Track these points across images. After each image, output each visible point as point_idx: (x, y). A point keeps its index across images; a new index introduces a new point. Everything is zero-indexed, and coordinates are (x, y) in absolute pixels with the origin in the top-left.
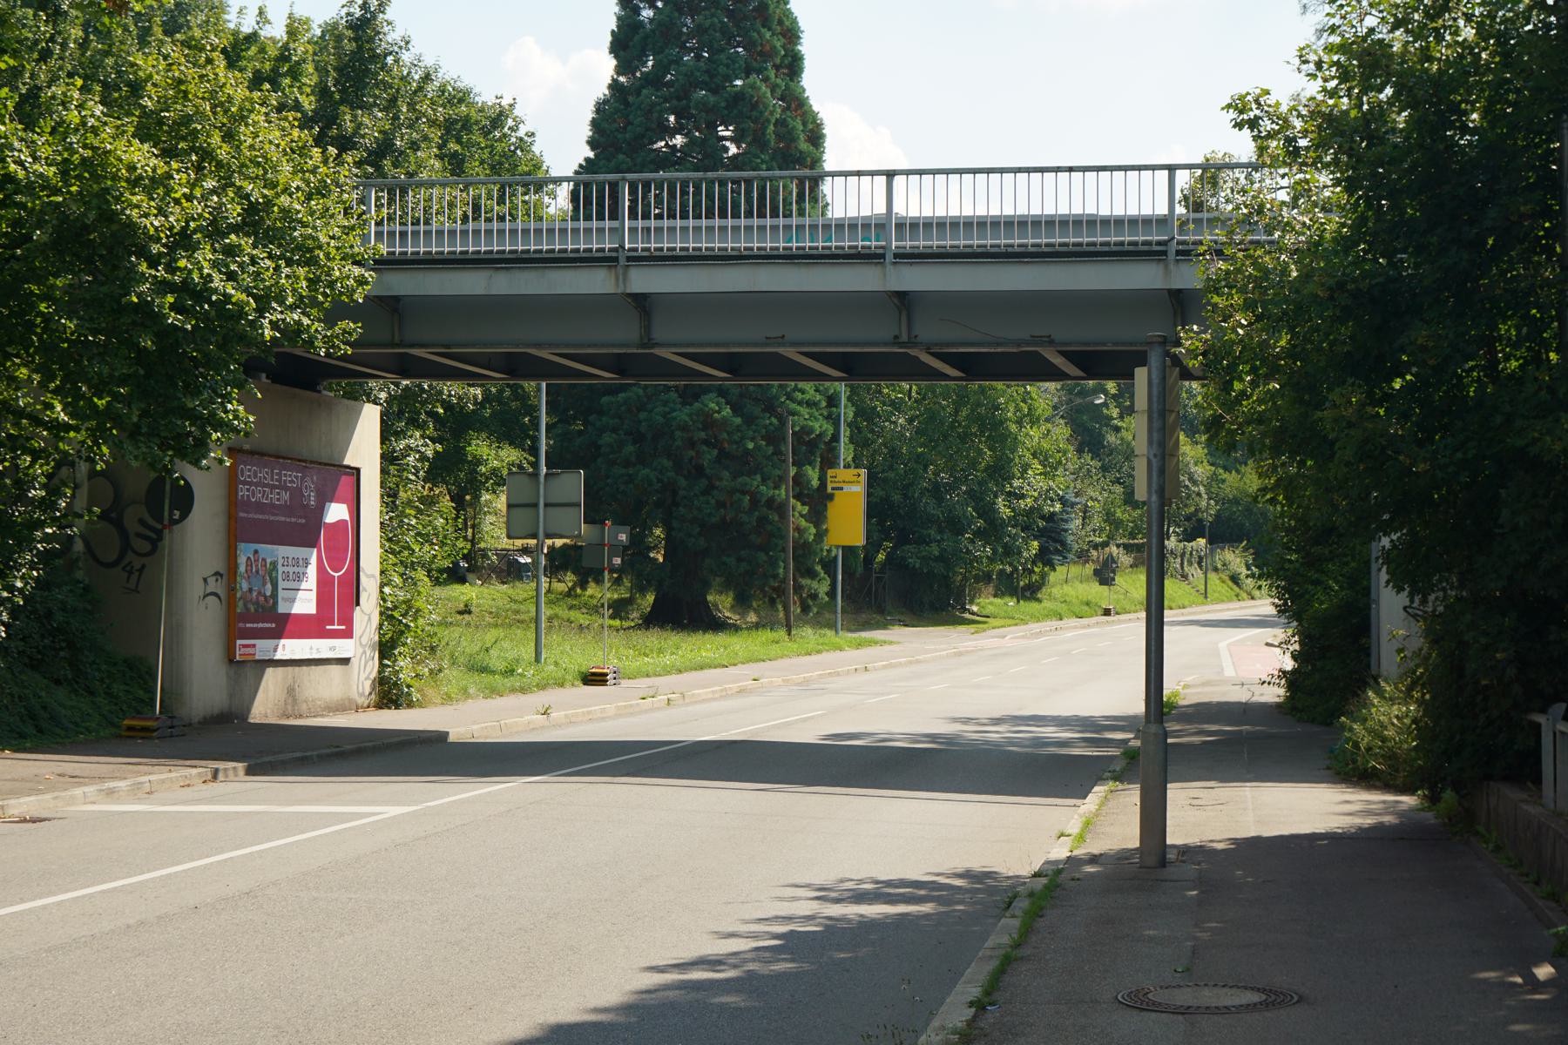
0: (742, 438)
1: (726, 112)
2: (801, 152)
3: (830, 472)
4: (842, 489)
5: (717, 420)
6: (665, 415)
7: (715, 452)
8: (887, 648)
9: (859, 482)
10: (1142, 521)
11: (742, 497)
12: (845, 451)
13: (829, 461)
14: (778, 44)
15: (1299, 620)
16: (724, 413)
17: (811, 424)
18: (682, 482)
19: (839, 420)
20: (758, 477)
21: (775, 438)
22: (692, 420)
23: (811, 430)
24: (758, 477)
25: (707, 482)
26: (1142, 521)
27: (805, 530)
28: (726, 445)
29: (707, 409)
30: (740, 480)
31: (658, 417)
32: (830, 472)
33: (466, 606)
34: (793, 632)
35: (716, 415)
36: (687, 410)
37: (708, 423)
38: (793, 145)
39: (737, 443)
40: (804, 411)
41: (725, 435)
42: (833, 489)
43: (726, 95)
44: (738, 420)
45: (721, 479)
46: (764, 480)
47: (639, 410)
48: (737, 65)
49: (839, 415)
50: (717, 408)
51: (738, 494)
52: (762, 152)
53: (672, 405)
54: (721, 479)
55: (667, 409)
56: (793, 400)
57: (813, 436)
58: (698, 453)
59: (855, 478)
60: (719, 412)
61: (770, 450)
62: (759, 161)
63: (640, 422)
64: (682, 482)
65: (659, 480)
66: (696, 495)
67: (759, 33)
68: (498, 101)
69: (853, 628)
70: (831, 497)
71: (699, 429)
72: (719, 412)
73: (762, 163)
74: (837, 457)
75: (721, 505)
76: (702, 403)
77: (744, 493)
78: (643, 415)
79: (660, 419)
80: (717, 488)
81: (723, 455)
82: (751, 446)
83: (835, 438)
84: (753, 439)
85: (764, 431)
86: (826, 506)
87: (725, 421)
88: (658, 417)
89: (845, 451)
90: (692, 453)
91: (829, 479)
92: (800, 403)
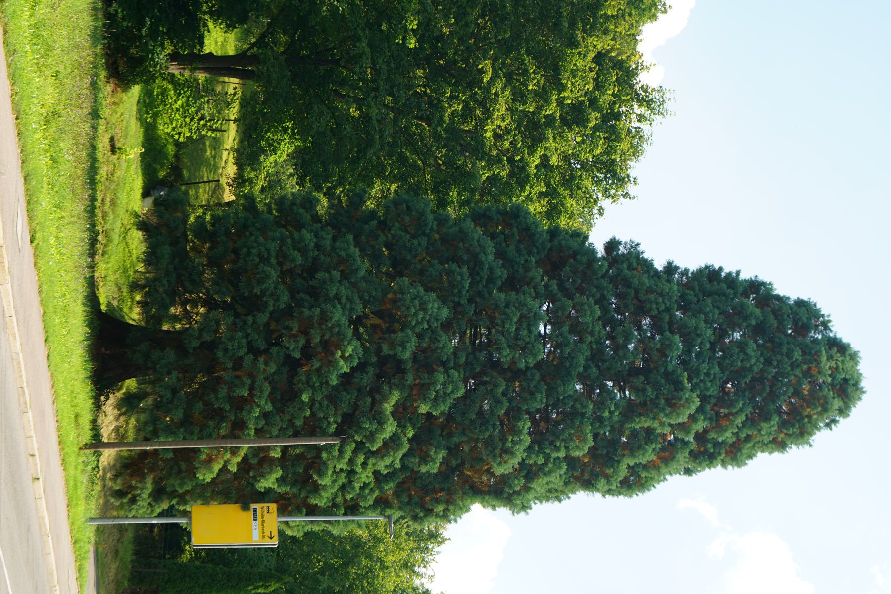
0: (313, 388)
1: (663, 370)
2: (619, 462)
3: (273, 507)
4: (255, 519)
5: (333, 354)
6: (337, 297)
7: (297, 355)
8: (73, 574)
9: (264, 537)
10: (522, 83)
11: (247, 386)
12: (299, 525)
13: (286, 506)
14: (728, 434)
15: (791, 307)
16: (341, 363)
17: (330, 472)
18: (263, 318)
19: (331, 515)
20: (269, 407)
21: (313, 428)
22: (332, 327)
23: (321, 474)
24: (269, 407)
25: (262, 348)
26: (522, 83)
27: (210, 470)
28: (305, 369)
29: (346, 343)
30: (266, 384)
31: (334, 288)
32: (273, 507)
33: (120, 149)
34: (87, 452)
35: (339, 354)
36: (344, 321)
37: (329, 347)
38: (626, 452)
39: (308, 382)
40: (343, 465)
41: (317, 365)
42: (255, 510)
43: (679, 371)
44: (334, 381)
45: (266, 363)
46: (265, 415)
47: (342, 272)
48: (709, 384)
49: (335, 515)
50: (347, 355)
51: (249, 382)
52: (620, 414)
53: (348, 307)
54: (266, 363)
55: (344, 300)
56: (355, 452)
57: (315, 477)
58: (295, 336)
59: (268, 533)
60: (342, 357)
61: (299, 423)
62: (613, 409)
63: (329, 272)
64: (263, 318)
65: (263, 292)
66: (247, 335)
67: (741, 410)
68: (632, 179)
69: (100, 550)
70: (245, 508)
71: (322, 336)
72: (342, 357)
73: (610, 412)
74: (290, 514)
75: (238, 363)
76: (351, 340)
77: (252, 388)
78: (336, 274)
79: (333, 291)
80: (256, 359)
81: (294, 366)
82: (305, 397)
83: (312, 511)
84: (312, 400)
85: (321, 415)
86: (236, 503)
87: (332, 364)
88: (334, 288)
89: (299, 525)
90: (296, 328)
91: (265, 505)
92: (351, 462)
